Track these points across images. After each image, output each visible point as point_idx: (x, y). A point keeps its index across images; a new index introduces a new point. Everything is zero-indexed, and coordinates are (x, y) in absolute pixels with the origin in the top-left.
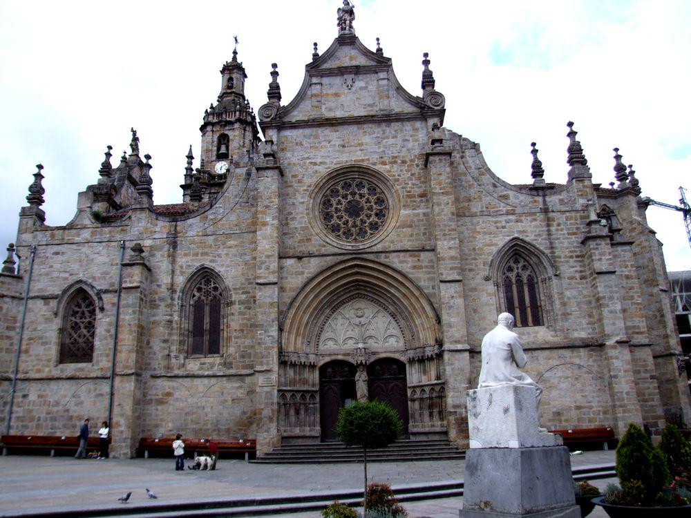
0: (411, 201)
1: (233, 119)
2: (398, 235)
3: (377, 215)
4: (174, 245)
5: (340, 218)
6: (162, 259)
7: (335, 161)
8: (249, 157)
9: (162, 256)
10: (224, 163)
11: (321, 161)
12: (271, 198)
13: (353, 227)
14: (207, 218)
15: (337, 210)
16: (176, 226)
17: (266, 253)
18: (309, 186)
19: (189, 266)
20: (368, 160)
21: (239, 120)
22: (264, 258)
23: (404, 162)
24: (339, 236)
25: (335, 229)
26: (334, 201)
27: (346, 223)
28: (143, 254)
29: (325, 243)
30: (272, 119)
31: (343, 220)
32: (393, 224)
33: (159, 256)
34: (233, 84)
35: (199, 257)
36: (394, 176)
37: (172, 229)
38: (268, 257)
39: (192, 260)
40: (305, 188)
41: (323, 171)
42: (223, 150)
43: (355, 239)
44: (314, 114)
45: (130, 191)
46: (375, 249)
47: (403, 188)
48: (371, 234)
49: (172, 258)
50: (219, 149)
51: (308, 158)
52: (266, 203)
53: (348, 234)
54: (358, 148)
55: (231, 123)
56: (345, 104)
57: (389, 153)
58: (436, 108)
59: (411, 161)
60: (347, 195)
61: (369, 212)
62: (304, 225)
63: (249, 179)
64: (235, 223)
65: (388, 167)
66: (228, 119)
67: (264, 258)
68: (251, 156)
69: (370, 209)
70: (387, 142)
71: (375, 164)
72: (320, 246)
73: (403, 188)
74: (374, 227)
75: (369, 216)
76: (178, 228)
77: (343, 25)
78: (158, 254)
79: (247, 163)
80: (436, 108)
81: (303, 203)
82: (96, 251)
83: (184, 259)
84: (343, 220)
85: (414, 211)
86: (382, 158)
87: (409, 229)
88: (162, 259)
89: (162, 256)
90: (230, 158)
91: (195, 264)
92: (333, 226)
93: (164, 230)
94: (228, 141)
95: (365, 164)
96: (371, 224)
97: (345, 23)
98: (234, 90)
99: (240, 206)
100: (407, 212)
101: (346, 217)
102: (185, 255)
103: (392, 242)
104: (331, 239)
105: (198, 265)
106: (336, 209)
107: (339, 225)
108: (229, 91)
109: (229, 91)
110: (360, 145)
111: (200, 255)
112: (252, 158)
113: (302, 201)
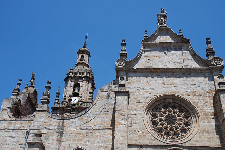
0: (206, 117)
1: (83, 76)
2: (200, 137)
3: (184, 124)
4: (61, 134)
5: (162, 124)
6: (53, 142)
7: (159, 92)
8: (109, 86)
9: (53, 140)
10: (76, 98)
11: (151, 91)
12: (123, 109)
13: (170, 130)
14: (83, 119)
15: (160, 120)
16: (63, 122)
17: (120, 141)
18: (145, 105)
19: (69, 147)
20: (179, 92)
21: (86, 77)
22: (118, 145)
23: (200, 95)
24: (162, 135)
25: (160, 130)
26: (158, 114)
27: (166, 128)
28: (41, 138)
29: (154, 139)
30: (123, 66)
31: (164, 126)
32: (196, 131)
33: (51, 140)
34: (83, 59)
35: (76, 142)
36: (195, 102)
37: (61, 123)
38: (122, 144)
39: (71, 143)
40: (142, 106)
41: (152, 97)
42: (76, 91)
43: (172, 138)
44: (147, 66)
45: (27, 105)
46: (186, 144)
47: (201, 109)
48: (182, 136)
49: (59, 142)
50: (74, 90)
51: (144, 89)
52: (121, 111)
53: (168, 134)
54: (172, 85)
55: (82, 78)
56: (164, 62)
57: (191, 90)
58: (218, 66)
59: (204, 94)
60: (166, 111)
61: (178, 126)
62: (141, 127)
63: (109, 98)
64: (100, 122)
65: (190, 97)
66: (80, 76)
67: (118, 145)
68: (110, 86)
69: (181, 120)
70: (189, 83)
71: (183, 95)
72: (151, 140)
73: (201, 109)
74: (184, 131)
75: (180, 125)
76: (64, 124)
77: (161, 22)
78: (50, 139)
79: (108, 89)
80: (218, 66)
81: (141, 114)
82: (9, 135)
83: (67, 143)
84: (164, 126)
85: (209, 123)
86: (187, 91)
87: (208, 134)
88: (53, 142)
89: (53, 140)
90: (80, 95)
91: (74, 146)
92: (158, 129)
93: (55, 124)
94: (79, 86)
95: (177, 94)
96: (181, 129)
97: (162, 22)
98: (84, 62)
99: (103, 113)
100: (204, 124)
101: (166, 124)
102: (68, 140)
103: (197, 141)
104: (157, 136)
105: (75, 147)
106: (160, 119)
107: (162, 129)
108: (81, 62)
109: (81, 62)
110: (173, 84)
111: (77, 141)
112: (111, 87)
113: (140, 112)
